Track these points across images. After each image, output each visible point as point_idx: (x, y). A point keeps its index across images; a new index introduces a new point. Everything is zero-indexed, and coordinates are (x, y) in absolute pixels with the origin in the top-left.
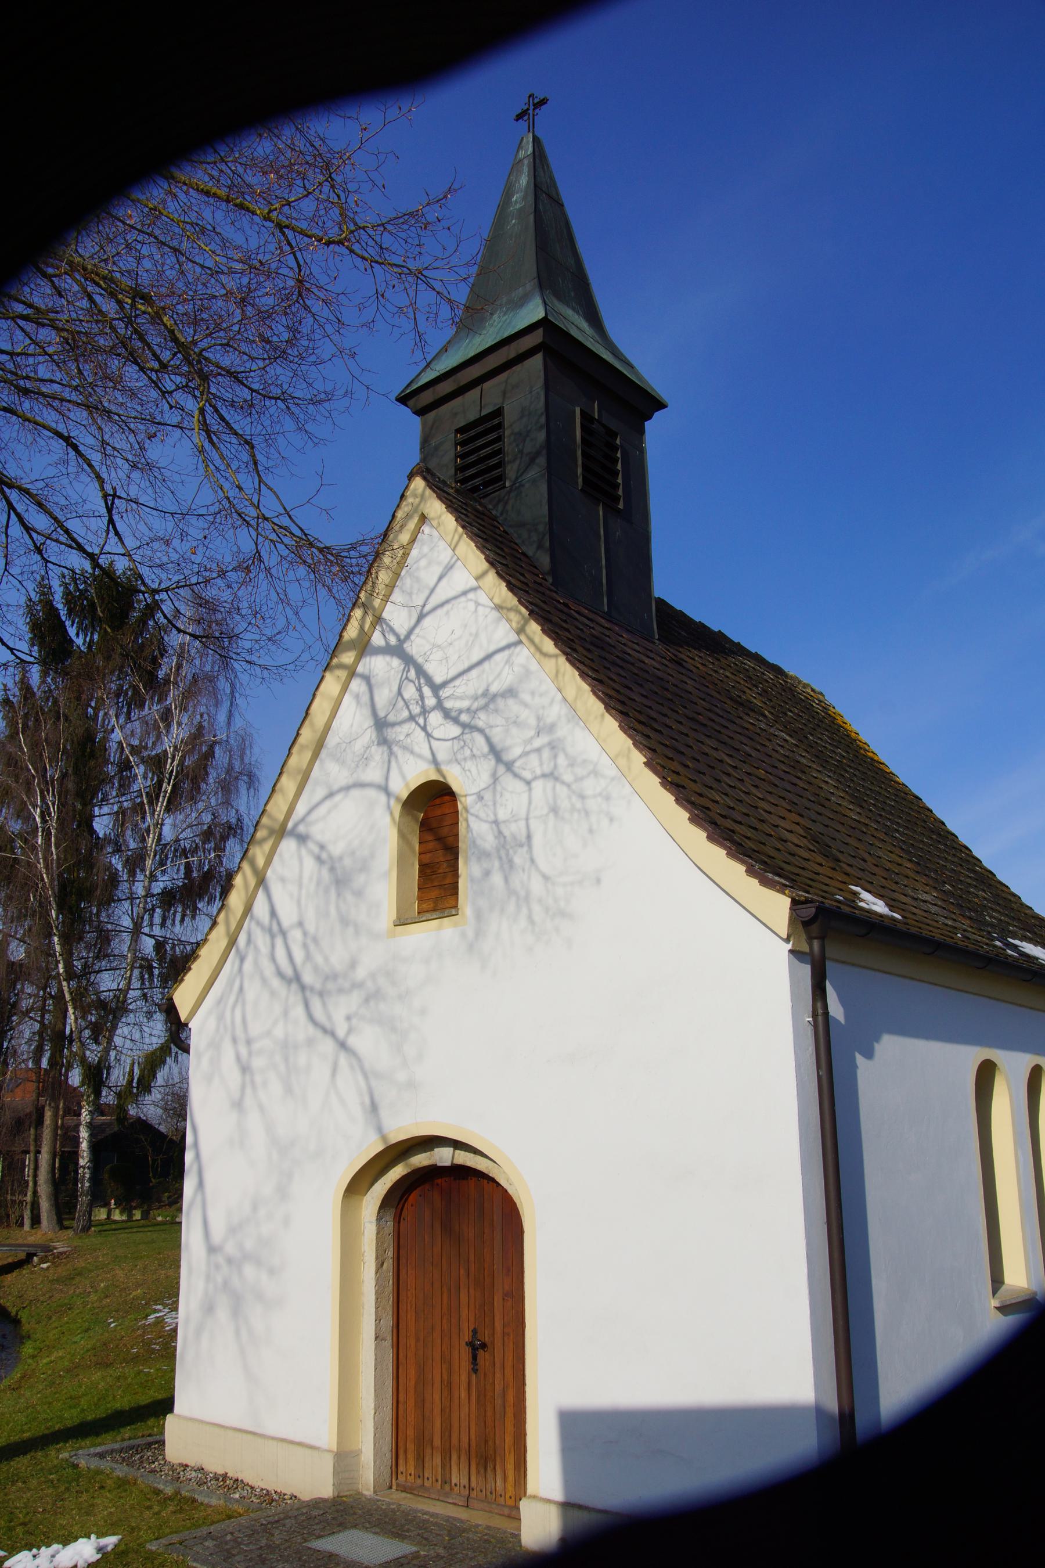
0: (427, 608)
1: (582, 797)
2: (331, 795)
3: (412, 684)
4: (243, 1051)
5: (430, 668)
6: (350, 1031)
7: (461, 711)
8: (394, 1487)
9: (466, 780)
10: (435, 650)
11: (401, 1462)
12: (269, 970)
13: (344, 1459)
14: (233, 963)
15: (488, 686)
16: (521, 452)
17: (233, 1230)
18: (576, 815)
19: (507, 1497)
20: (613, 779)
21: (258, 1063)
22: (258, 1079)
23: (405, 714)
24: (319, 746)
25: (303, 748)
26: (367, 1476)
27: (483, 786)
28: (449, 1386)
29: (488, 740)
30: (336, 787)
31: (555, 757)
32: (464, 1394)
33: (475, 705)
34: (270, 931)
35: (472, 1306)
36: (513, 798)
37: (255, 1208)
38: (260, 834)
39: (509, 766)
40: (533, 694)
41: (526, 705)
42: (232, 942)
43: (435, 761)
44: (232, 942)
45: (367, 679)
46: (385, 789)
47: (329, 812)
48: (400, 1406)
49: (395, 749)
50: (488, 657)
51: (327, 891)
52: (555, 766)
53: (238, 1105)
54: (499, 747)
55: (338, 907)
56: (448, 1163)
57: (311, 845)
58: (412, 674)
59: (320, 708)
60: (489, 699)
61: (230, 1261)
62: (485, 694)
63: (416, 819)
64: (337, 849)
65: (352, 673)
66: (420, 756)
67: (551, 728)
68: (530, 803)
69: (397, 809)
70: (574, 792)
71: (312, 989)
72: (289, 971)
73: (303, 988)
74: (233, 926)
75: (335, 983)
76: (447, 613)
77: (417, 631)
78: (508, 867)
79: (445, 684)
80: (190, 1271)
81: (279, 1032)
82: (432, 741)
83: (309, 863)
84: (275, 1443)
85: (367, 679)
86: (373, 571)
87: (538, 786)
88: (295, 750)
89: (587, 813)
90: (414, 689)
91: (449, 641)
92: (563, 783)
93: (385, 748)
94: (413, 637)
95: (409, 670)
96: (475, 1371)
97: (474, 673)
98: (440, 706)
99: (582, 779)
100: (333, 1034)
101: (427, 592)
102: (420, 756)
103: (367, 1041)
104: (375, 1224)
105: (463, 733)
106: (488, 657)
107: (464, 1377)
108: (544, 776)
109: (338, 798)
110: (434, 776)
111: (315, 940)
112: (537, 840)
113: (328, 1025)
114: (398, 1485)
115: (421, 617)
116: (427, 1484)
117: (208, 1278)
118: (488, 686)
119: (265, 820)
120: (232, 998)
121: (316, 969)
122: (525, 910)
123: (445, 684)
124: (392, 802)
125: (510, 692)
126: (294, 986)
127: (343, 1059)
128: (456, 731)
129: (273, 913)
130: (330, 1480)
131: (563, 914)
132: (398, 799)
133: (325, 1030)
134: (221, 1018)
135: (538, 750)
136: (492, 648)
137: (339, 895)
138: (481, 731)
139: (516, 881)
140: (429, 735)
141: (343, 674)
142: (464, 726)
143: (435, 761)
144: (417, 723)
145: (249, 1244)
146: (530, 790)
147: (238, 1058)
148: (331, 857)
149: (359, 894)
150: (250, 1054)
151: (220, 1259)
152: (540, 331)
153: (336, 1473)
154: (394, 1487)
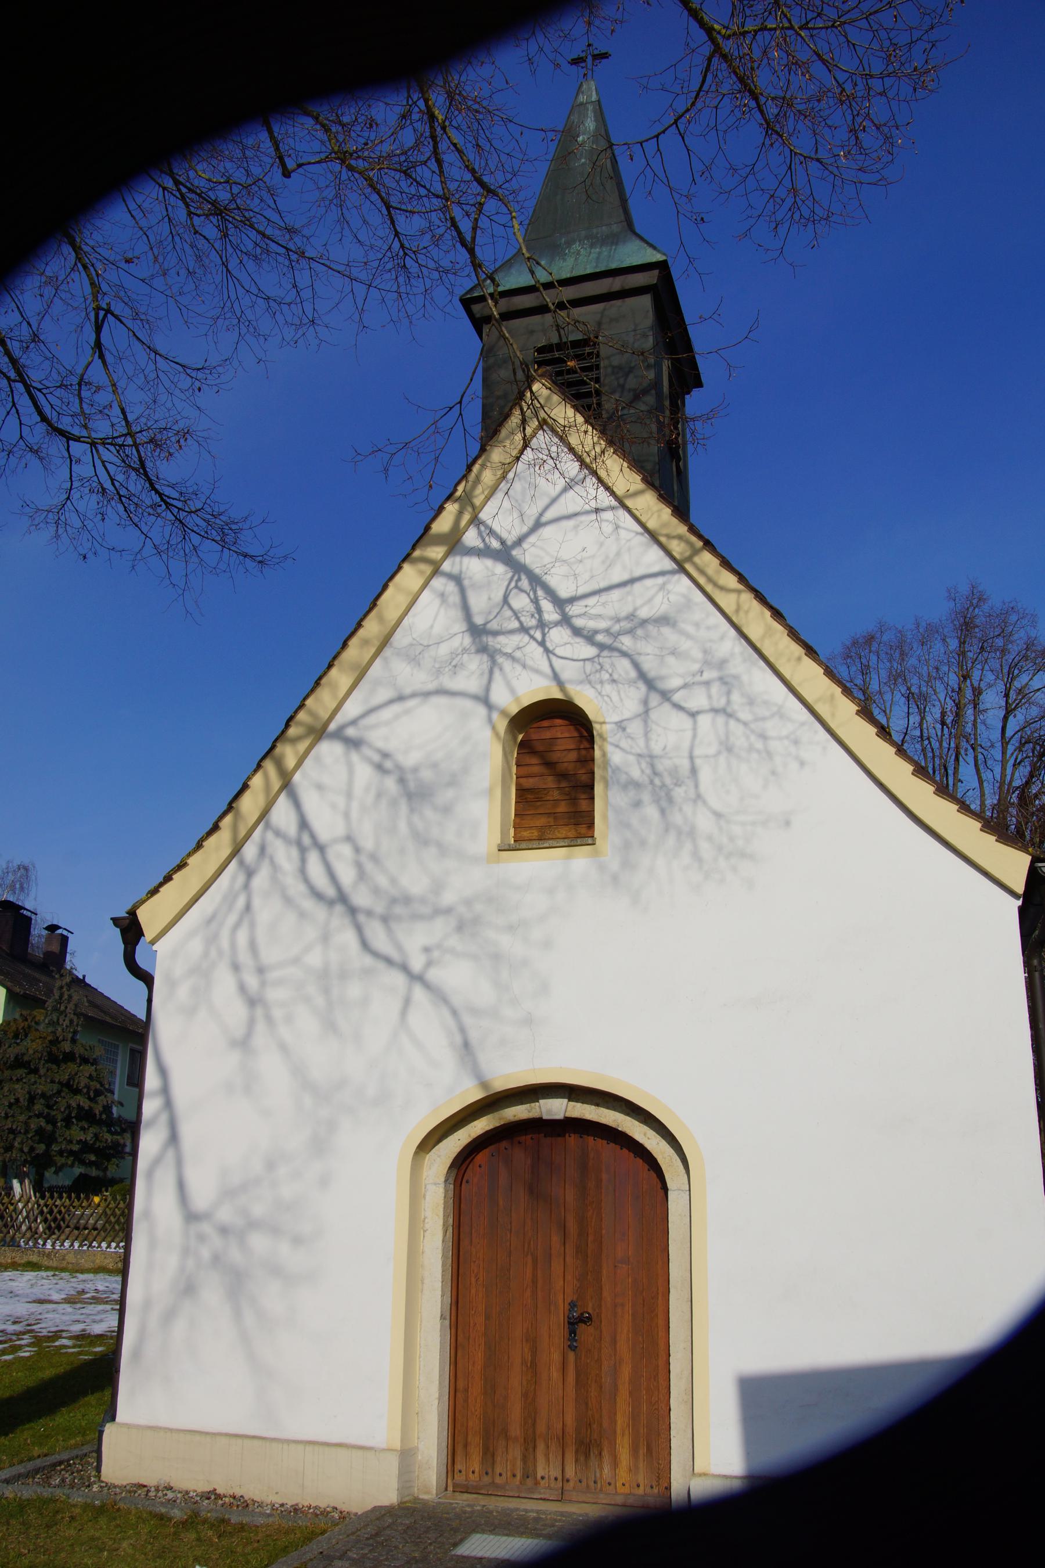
0: (549, 515)
1: (763, 737)
2: (401, 698)
3: (524, 595)
4: (252, 981)
5: (552, 581)
6: (429, 964)
7: (596, 632)
8: (450, 1488)
9: (606, 704)
10: (557, 564)
11: (458, 1458)
12: (296, 888)
13: (406, 1455)
14: (234, 879)
15: (635, 610)
16: (622, 387)
17: (229, 1193)
18: (755, 756)
20: (803, 724)
21: (273, 995)
22: (277, 1013)
23: (516, 624)
24: (385, 641)
25: (366, 642)
26: (429, 1477)
27: (627, 715)
28: (533, 1368)
29: (636, 665)
30: (408, 691)
31: (729, 693)
32: (556, 1375)
33: (617, 628)
34: (299, 844)
35: (569, 1277)
36: (670, 732)
37: (271, 1165)
38: (292, 731)
39: (666, 696)
40: (697, 625)
41: (688, 636)
42: (236, 851)
43: (556, 676)
44: (236, 851)
45: (457, 579)
46: (484, 700)
47: (397, 717)
48: (459, 1395)
49: (500, 660)
50: (632, 581)
51: (394, 803)
52: (729, 702)
53: (243, 1043)
54: (652, 674)
55: (410, 824)
56: (560, 1116)
57: (366, 751)
58: (525, 583)
59: (392, 600)
60: (636, 624)
61: (224, 1230)
62: (631, 617)
63: (515, 738)
64: (409, 760)
65: (436, 571)
66: (537, 671)
67: (722, 663)
68: (695, 736)
69: (502, 725)
70: (753, 731)
71: (369, 913)
72: (330, 892)
73: (352, 911)
74: (242, 833)
75: (398, 908)
76: (576, 527)
77: (532, 539)
78: (665, 800)
79: (572, 600)
80: (153, 1244)
81: (315, 959)
82: (554, 659)
83: (364, 773)
84: (301, 1447)
85: (457, 579)
86: (476, 468)
87: (704, 720)
88: (353, 642)
89: (769, 755)
90: (528, 600)
91: (579, 557)
92: (738, 720)
93: (485, 658)
94: (525, 545)
95: (519, 579)
96: (573, 1348)
97: (615, 594)
98: (566, 620)
99: (764, 719)
100: (405, 968)
101: (546, 501)
102: (537, 671)
103: (456, 976)
104: (443, 1185)
105: (598, 656)
106: (632, 581)
107: (556, 1357)
108: (715, 711)
109: (411, 703)
110: (558, 695)
111: (374, 858)
112: (705, 775)
113: (395, 955)
114: (455, 1485)
115: (538, 525)
116: (498, 1480)
117: (186, 1251)
118: (635, 610)
119: (302, 716)
120: (232, 919)
121: (376, 891)
122: (688, 846)
123: (572, 600)
124: (495, 716)
125: (664, 620)
126: (339, 908)
127: (419, 993)
128: (590, 651)
129: (304, 824)
130: (394, 1484)
131: (743, 855)
132: (503, 713)
133: (389, 961)
134: (212, 940)
135: (707, 684)
136: (638, 573)
137: (412, 810)
138: (624, 654)
139: (677, 818)
140: (547, 651)
141: (428, 569)
142: (602, 647)
143: (556, 676)
144: (532, 637)
145: (258, 1210)
146: (695, 722)
147: (242, 988)
148: (399, 768)
149: (447, 810)
150: (263, 984)
151: (206, 1228)
152: (656, 272)
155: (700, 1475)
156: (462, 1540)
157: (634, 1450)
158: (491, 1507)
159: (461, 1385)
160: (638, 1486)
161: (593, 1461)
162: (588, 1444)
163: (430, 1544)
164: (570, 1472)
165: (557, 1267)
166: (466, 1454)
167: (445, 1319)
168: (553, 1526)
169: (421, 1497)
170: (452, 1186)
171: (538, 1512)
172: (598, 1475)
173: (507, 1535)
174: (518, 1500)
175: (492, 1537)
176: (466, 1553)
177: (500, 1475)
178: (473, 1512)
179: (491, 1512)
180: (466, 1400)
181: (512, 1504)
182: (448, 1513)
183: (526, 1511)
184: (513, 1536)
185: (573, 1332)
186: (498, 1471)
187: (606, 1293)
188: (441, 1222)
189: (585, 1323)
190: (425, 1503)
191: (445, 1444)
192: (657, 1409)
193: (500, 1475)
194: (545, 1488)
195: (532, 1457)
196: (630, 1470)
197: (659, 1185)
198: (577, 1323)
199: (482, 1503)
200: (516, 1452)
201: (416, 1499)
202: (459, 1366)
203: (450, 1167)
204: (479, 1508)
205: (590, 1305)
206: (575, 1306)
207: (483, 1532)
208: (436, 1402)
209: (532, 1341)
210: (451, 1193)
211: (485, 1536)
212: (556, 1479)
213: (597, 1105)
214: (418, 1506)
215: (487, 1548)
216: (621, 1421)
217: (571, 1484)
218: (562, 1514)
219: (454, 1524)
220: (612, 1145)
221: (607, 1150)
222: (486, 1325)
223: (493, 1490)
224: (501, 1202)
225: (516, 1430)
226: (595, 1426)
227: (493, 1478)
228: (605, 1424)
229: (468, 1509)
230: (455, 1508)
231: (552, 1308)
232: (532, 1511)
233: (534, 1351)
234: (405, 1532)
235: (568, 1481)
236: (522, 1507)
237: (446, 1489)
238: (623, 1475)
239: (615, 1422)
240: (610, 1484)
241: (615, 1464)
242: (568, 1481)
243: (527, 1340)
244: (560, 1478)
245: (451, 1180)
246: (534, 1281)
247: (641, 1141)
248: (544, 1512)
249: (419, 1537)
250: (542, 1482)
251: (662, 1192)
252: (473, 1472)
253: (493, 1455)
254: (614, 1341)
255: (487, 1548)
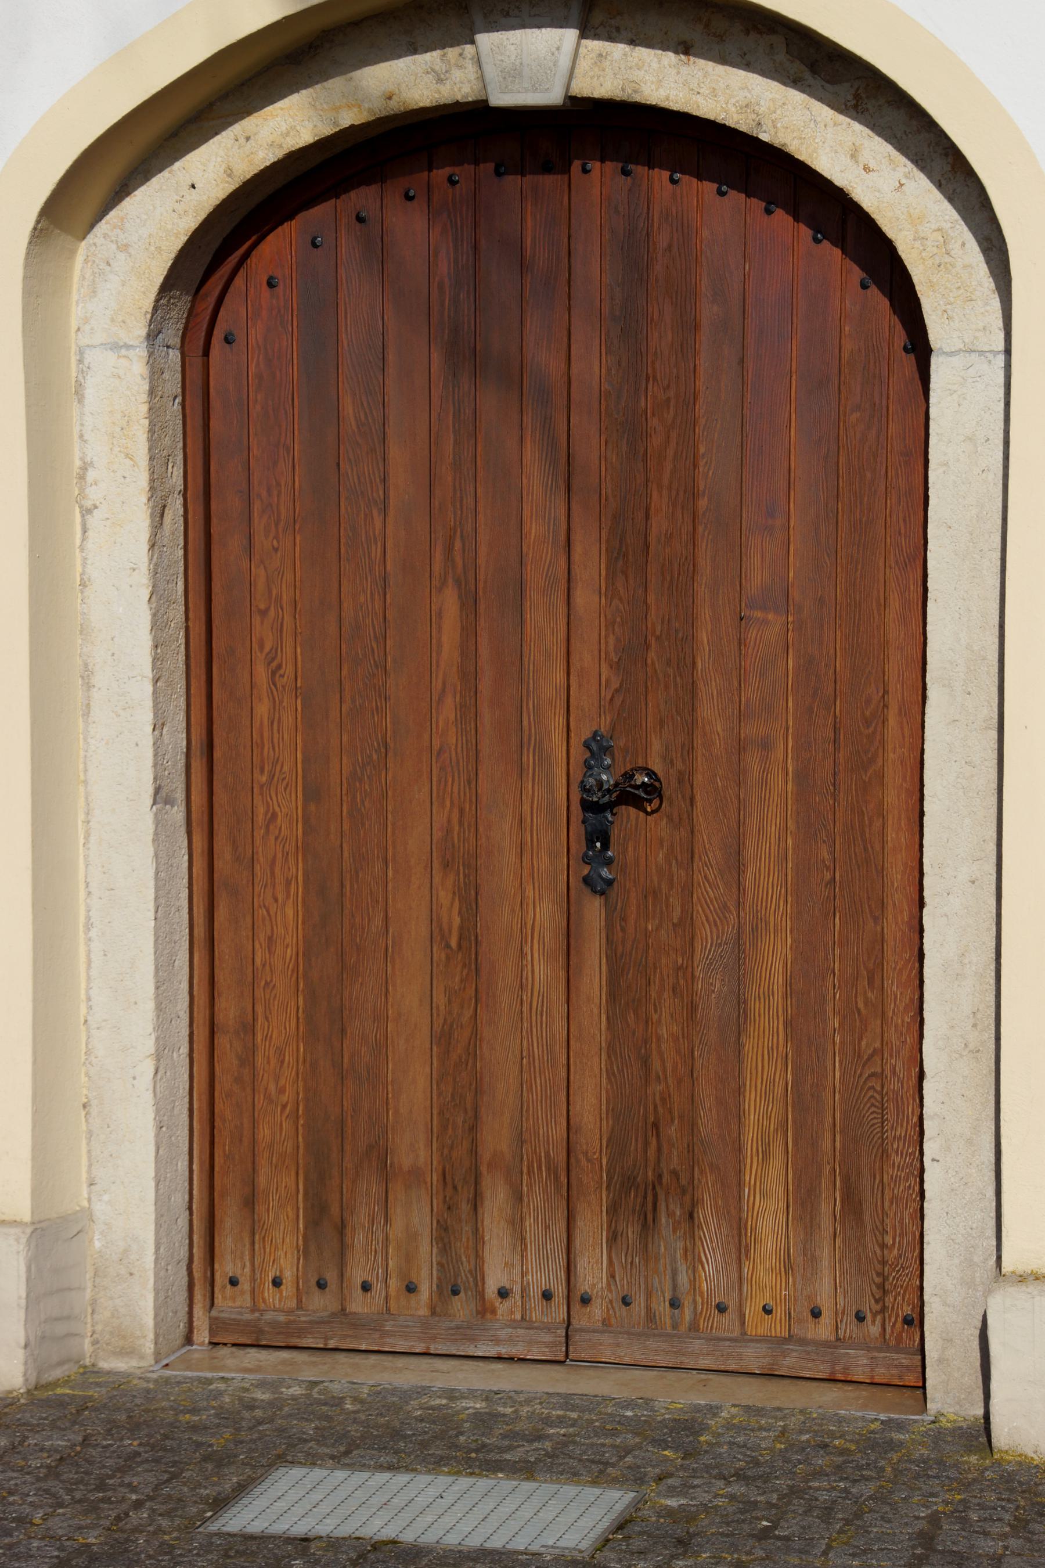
8: (202, 1336)
11: (226, 1242)
13: (52, 1238)
19: (752, 1309)
26: (130, 1293)
28: (466, 950)
32: (542, 971)
35: (585, 656)
48: (223, 1041)
56: (552, 96)
107: (544, 914)
114: (216, 1326)
116: (359, 1305)
130: (14, 1329)
153: (34, 1300)
154: (202, 1336)
155: (1022, 1279)
156: (242, 1489)
157: (803, 1201)
158: (335, 1388)
159: (229, 1009)
160: (816, 1314)
161: (669, 1240)
162: (650, 1184)
163: (138, 1505)
164: (592, 1273)
165: (542, 622)
166: (254, 1229)
167: (169, 801)
168: (539, 1438)
169: (104, 1365)
170: (175, 355)
171: (488, 1396)
172: (683, 1279)
173: (390, 1468)
174: (425, 1362)
175: (340, 1475)
176: (256, 1527)
177: (366, 1287)
178: (275, 1405)
179: (339, 1401)
180: (248, 1059)
181: (406, 1375)
182: (194, 1411)
183: (451, 1395)
184: (408, 1469)
185: (599, 837)
186: (357, 1274)
187: (711, 712)
188: (142, 479)
189: (638, 803)
190: (119, 1383)
191: (180, 1199)
192: (881, 1075)
193: (366, 1287)
194: (514, 1324)
195: (467, 1228)
196: (788, 1267)
197: (900, 337)
198: (611, 806)
199: (309, 1375)
200: (415, 1215)
201: (89, 1373)
202: (222, 948)
203: (168, 286)
204: (296, 1390)
205: (656, 745)
206: (606, 750)
207: (312, 1461)
208: (149, 1066)
209: (463, 864)
210: (172, 382)
211: (318, 1473)
212: (547, 1296)
213: (685, 49)
214: (93, 1393)
215: (325, 1508)
216: (761, 1111)
217: (597, 1310)
218: (567, 1401)
219: (217, 1443)
220: (734, 197)
221: (715, 214)
222: (306, 820)
223: (343, 1336)
224: (348, 408)
225: (413, 1147)
226: (672, 1131)
227: (343, 1299)
228: (708, 1123)
229: (261, 1395)
230: (220, 1393)
231: (529, 758)
232: (472, 1394)
233: (470, 898)
234: (52, 1472)
235: (585, 1301)
236: (439, 1383)
237: (189, 1340)
238: (765, 1279)
239: (740, 1116)
240: (721, 1309)
241: (740, 1243)
242: (585, 1301)
243: (446, 865)
244: (559, 1291)
245: (172, 334)
246: (469, 676)
247: (839, 179)
248: (509, 1398)
249: (101, 1487)
250: (503, 1308)
251: (908, 363)
252: (277, 1283)
253: (341, 1229)
254: (736, 863)
255: (325, 1508)
